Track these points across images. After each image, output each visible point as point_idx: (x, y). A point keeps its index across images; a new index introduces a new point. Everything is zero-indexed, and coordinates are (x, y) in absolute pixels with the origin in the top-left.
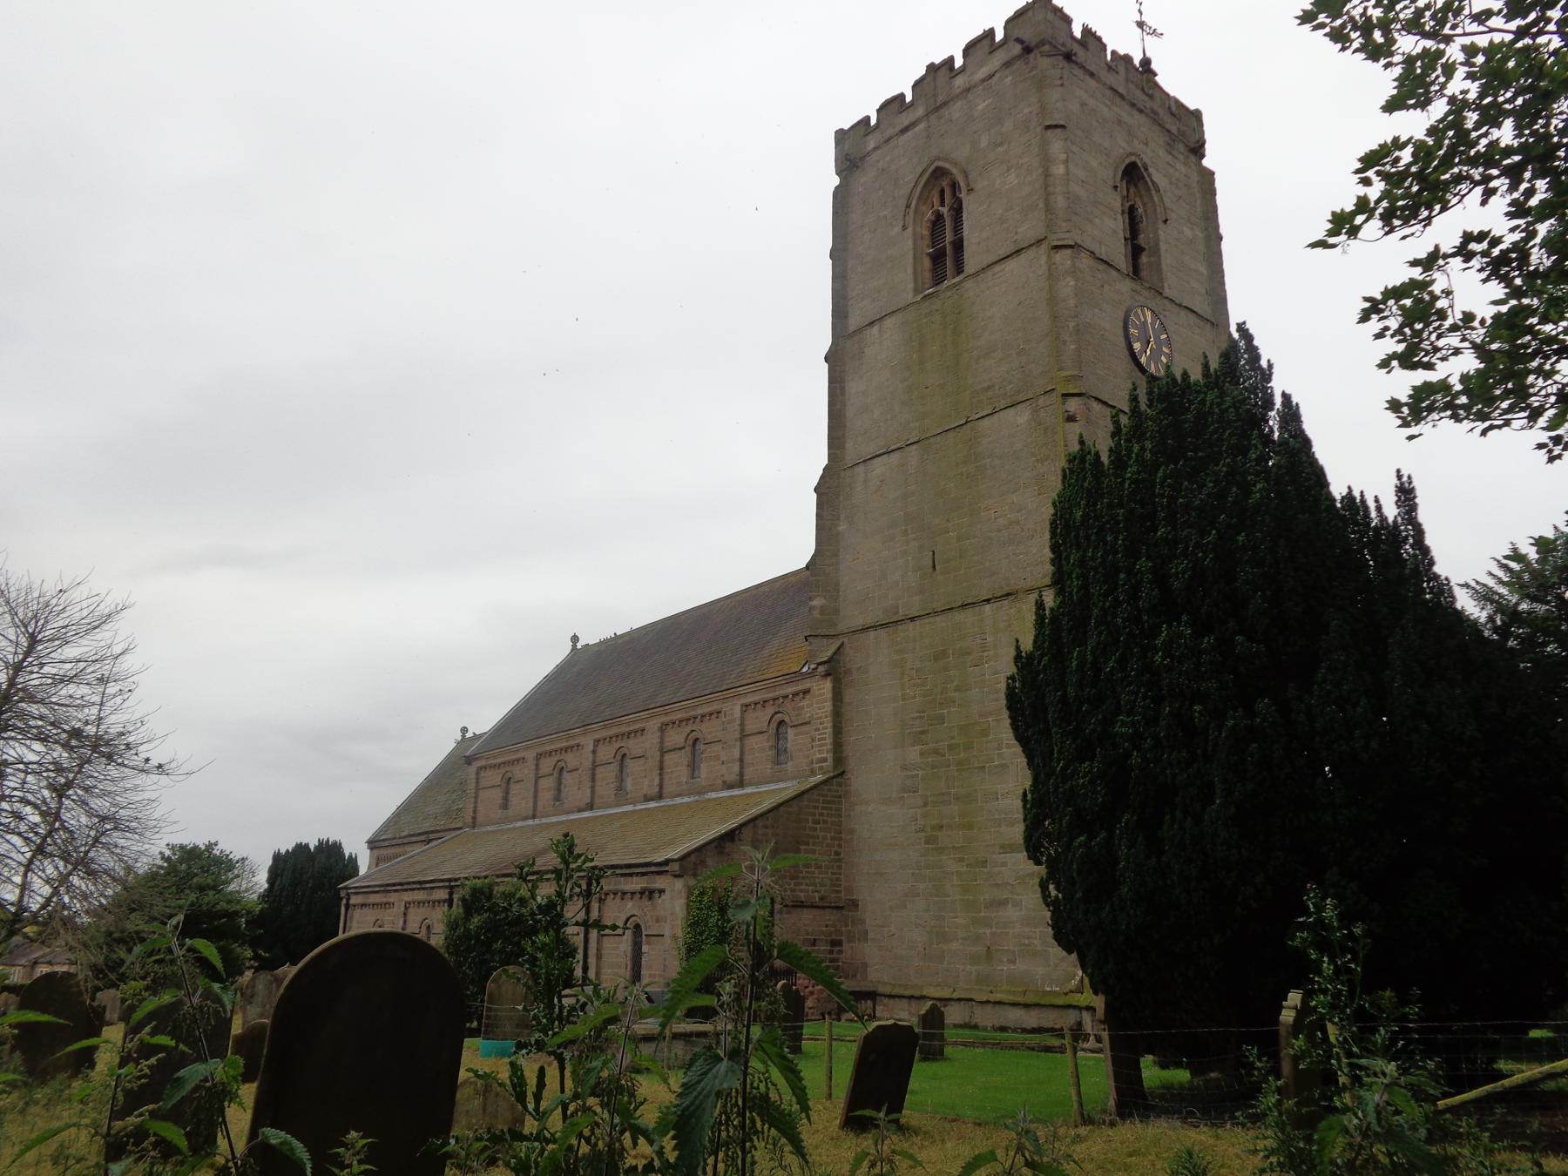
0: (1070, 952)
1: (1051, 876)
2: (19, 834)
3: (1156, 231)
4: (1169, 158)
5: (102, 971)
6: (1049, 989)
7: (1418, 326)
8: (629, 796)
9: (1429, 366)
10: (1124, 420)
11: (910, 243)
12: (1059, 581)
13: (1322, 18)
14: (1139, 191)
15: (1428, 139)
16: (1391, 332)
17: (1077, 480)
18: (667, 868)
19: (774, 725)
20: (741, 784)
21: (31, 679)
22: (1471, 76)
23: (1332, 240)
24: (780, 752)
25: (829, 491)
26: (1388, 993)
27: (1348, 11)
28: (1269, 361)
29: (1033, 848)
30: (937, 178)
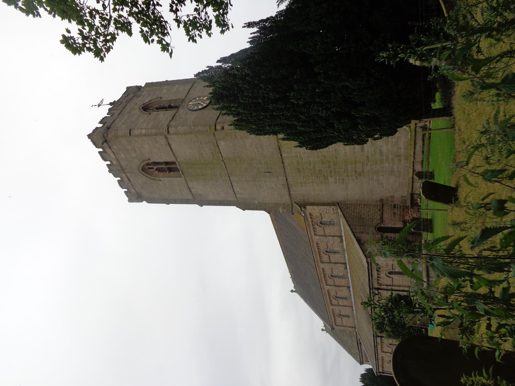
0: (397, 131)
1: (372, 136)
6: (409, 137)
7: (198, 25)
8: (345, 274)
9: (211, 21)
11: (165, 179)
12: (275, 133)
13: (102, 55)
14: (151, 106)
16: (200, 33)
18: (370, 262)
19: (321, 225)
20: (341, 237)
22: (122, 10)
23: (170, 51)
24: (331, 223)
25: (245, 206)
27: (101, 47)
28: (206, 67)
29: (363, 142)
30: (145, 170)
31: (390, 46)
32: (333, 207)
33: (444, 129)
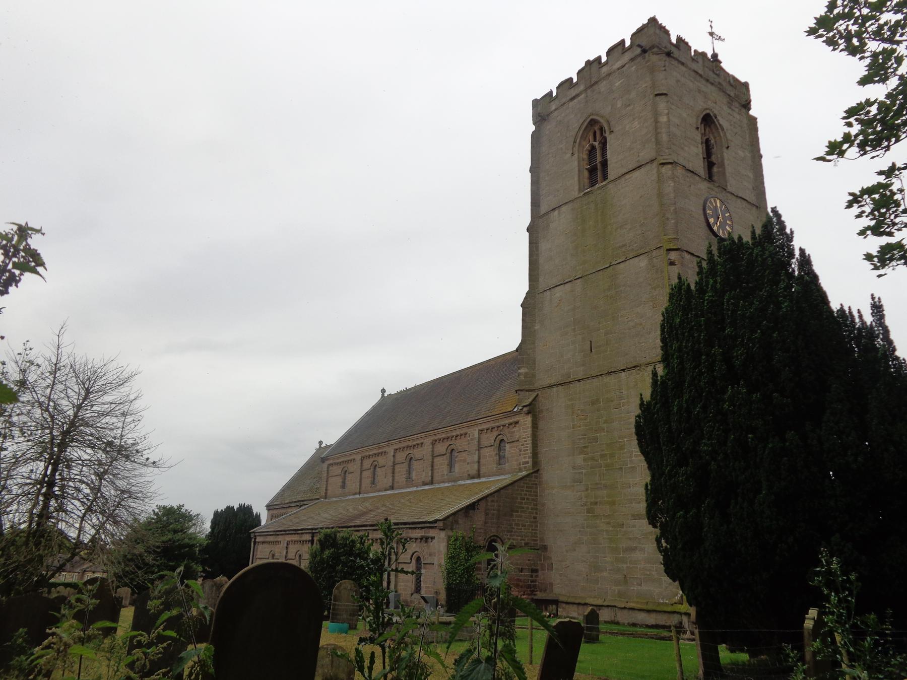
0: (674, 581)
1: (663, 534)
2: (79, 500)
4: (729, 111)
5: (121, 577)
6: (662, 601)
7: (883, 211)
9: (890, 234)
10: (704, 264)
11: (576, 163)
13: (821, 31)
15: (886, 100)
16: (866, 214)
17: (676, 301)
19: (498, 442)
21: (87, 414)
23: (828, 157)
24: (501, 458)
25: (529, 307)
26: (872, 616)
27: (837, 27)
28: (791, 229)
30: (591, 125)
31: (853, 578)
32: (530, 464)
33: (681, 665)
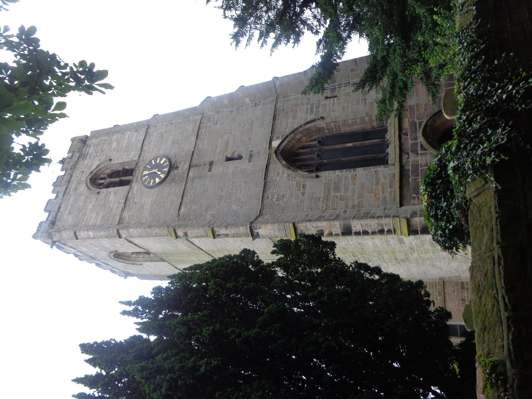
3: (116, 164)
14: (102, 173)
